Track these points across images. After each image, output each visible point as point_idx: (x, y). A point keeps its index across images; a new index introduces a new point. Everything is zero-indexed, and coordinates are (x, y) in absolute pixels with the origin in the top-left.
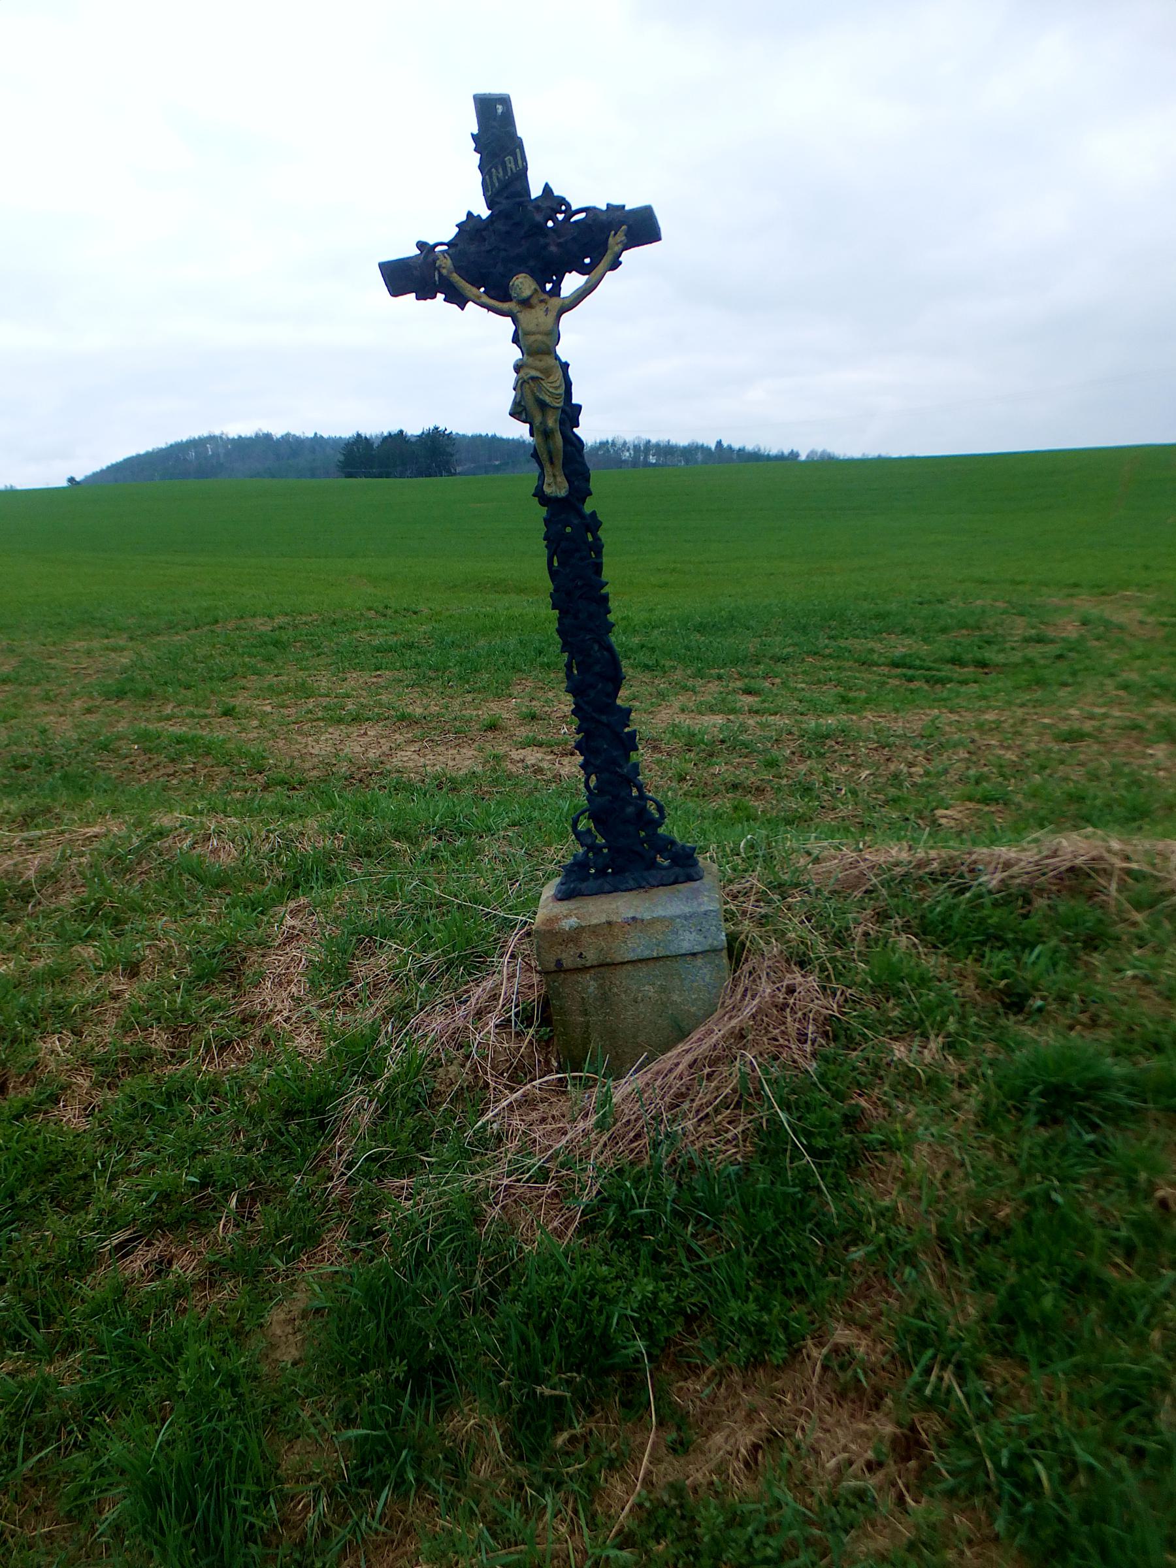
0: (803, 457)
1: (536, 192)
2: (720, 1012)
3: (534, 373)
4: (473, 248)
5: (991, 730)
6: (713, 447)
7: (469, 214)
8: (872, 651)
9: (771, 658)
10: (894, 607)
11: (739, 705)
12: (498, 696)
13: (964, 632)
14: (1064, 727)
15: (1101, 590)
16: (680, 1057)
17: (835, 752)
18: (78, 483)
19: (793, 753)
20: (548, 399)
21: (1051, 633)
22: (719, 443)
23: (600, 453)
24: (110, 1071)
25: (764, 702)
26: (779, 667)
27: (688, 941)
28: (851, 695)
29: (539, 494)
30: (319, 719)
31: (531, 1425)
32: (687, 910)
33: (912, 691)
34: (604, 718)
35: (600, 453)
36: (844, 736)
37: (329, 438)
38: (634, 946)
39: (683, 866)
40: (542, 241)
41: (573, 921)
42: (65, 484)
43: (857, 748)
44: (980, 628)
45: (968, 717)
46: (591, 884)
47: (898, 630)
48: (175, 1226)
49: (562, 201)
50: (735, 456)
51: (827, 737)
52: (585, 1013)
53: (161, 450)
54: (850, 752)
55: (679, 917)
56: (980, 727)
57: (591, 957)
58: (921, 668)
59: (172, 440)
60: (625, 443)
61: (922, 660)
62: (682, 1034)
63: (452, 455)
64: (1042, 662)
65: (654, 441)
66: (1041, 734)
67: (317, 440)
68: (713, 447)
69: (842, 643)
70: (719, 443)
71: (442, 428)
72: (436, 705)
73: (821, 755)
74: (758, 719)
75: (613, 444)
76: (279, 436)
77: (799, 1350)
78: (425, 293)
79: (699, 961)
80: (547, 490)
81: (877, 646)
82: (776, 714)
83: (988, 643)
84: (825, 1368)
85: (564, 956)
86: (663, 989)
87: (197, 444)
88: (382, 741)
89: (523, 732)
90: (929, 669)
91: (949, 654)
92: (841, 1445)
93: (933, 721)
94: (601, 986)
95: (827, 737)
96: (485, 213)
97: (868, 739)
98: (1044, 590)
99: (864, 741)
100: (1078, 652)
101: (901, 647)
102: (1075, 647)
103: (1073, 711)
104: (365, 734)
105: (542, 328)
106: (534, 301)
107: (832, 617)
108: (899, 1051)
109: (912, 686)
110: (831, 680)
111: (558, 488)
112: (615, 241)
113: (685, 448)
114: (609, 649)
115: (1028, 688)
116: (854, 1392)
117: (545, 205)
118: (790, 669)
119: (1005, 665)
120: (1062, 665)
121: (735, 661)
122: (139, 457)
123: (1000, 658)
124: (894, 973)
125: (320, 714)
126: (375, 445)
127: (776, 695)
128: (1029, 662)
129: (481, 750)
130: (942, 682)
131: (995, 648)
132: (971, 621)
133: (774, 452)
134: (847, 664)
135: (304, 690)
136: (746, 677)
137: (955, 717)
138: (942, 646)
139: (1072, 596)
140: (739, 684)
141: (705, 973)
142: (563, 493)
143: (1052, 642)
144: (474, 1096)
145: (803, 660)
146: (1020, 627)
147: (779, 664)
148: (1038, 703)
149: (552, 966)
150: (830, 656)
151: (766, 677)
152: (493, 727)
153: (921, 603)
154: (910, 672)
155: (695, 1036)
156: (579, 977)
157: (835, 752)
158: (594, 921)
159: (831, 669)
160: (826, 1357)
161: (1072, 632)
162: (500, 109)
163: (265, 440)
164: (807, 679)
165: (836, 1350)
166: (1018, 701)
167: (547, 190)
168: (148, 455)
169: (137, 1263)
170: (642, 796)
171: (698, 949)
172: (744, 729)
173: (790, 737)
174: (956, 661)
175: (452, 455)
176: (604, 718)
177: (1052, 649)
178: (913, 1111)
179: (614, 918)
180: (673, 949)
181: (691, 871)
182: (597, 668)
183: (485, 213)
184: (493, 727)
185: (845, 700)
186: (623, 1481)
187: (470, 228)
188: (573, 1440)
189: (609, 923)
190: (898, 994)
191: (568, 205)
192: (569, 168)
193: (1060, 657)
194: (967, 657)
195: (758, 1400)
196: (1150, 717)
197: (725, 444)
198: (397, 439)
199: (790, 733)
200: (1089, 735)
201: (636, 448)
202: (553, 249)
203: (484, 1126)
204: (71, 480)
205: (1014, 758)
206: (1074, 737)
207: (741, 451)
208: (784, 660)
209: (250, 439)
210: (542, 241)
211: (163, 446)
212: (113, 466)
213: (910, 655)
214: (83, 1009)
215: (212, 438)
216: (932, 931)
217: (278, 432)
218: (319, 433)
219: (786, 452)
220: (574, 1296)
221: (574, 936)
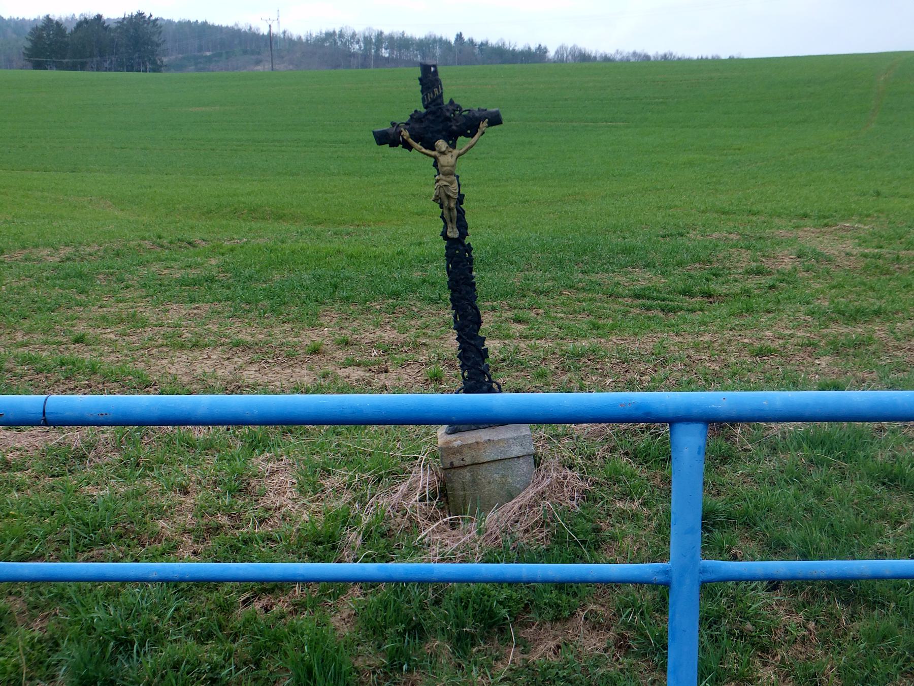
0: (551, 54)
1: (446, 101)
2: (532, 485)
3: (445, 183)
5: (704, 348)
6: (453, 40)
8: (618, 284)
9: (534, 292)
10: (638, 242)
11: (511, 332)
12: (312, 326)
13: (697, 265)
14: (757, 345)
15: (825, 220)
16: (514, 505)
17: (587, 366)
19: (557, 368)
21: (768, 265)
22: (459, 37)
23: (327, 44)
25: (531, 329)
26: (543, 299)
27: (516, 451)
28: (601, 322)
29: (444, 235)
30: (162, 346)
33: (650, 319)
34: (472, 342)
35: (327, 44)
36: (594, 354)
37: (10, 20)
38: (490, 454)
40: (449, 124)
41: (459, 442)
43: (603, 363)
44: (710, 262)
45: (690, 339)
47: (641, 264)
49: (458, 106)
50: (477, 51)
51: (582, 355)
54: (599, 366)
56: (696, 347)
57: (468, 460)
58: (657, 299)
60: (354, 35)
61: (658, 291)
62: (511, 497)
63: (158, 45)
64: (757, 292)
65: (386, 32)
66: (740, 351)
68: (453, 40)
69: (594, 277)
70: (459, 37)
72: (260, 333)
73: (578, 369)
74: (528, 342)
75: (341, 35)
77: (574, 614)
78: (394, 144)
79: (521, 461)
80: (449, 234)
81: (623, 279)
82: (541, 339)
83: (715, 275)
84: (586, 619)
85: (454, 460)
86: (503, 476)
88: (226, 363)
89: (342, 355)
90: (664, 300)
91: (681, 286)
92: (592, 644)
93: (661, 343)
95: (582, 355)
97: (613, 357)
98: (776, 220)
99: (609, 358)
100: (788, 283)
101: (644, 279)
102: (787, 278)
103: (768, 333)
104: (209, 357)
105: (451, 164)
107: (584, 253)
108: (619, 505)
109: (650, 314)
110: (584, 310)
111: (454, 233)
112: (483, 125)
113: (421, 41)
114: (476, 308)
115: (741, 315)
116: (596, 627)
117: (451, 108)
118: (551, 301)
119: (726, 295)
120: (772, 294)
121: (504, 295)
123: (723, 289)
124: (617, 471)
125: (160, 341)
127: (541, 323)
128: (747, 292)
129: (311, 369)
130: (674, 310)
131: (721, 279)
132: (703, 256)
133: (520, 46)
134: (597, 296)
136: (515, 308)
137: (677, 339)
138: (677, 279)
139: (797, 227)
140: (509, 314)
141: (525, 466)
142: (456, 236)
143: (770, 273)
144: (413, 527)
145: (561, 293)
146: (745, 260)
147: (541, 297)
148: (743, 327)
149: (448, 466)
150: (584, 289)
151: (531, 308)
153: (663, 237)
154: (649, 302)
155: (521, 495)
157: (587, 366)
159: (584, 301)
161: (787, 265)
162: (432, 69)
164: (565, 310)
166: (729, 326)
167: (452, 102)
169: (257, 606)
170: (490, 381)
171: (521, 454)
172: (518, 351)
173: (554, 356)
174: (688, 293)
175: (158, 45)
176: (472, 342)
177: (766, 280)
178: (627, 527)
179: (479, 440)
180: (509, 455)
182: (470, 318)
183: (423, 110)
184: (316, 351)
185: (596, 327)
186: (502, 664)
187: (416, 118)
188: (479, 651)
189: (477, 443)
190: (619, 481)
191: (461, 109)
193: (772, 287)
194: (696, 289)
196: (823, 337)
197: (466, 37)
198: (93, 26)
199: (554, 353)
200: (776, 351)
201: (367, 40)
202: (454, 127)
203: (421, 539)
205: (717, 368)
206: (763, 353)
207: (484, 45)
208: (546, 293)
210: (449, 124)
213: (649, 288)
219: (533, 47)
220: (477, 594)
221: (459, 450)
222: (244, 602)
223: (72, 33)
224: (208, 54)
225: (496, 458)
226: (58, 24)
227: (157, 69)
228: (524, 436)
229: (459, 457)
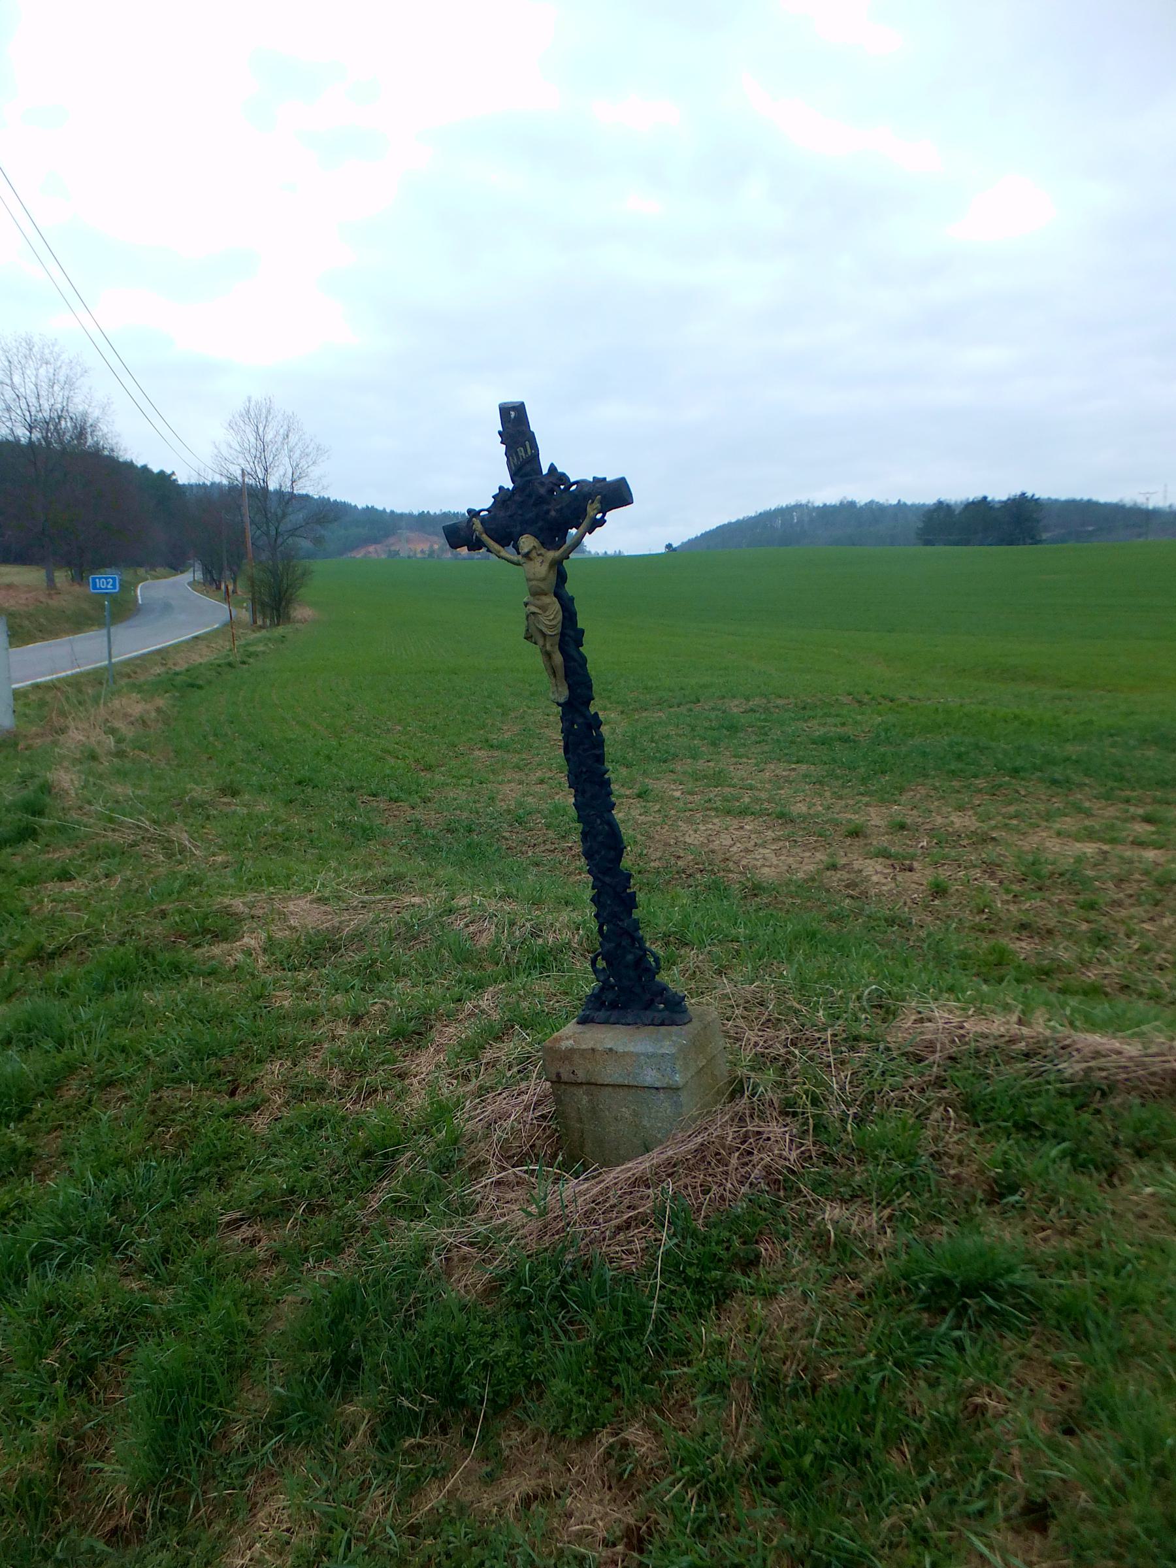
4: (502, 514)
7: (501, 488)
18: (675, 550)
20: (545, 630)
24: (300, 1093)
31: (392, 1425)
32: (651, 1050)
37: (913, 505)
38: (611, 1073)
39: (666, 1009)
42: (662, 550)
46: (602, 1014)
48: (266, 1215)
52: (580, 1121)
53: (751, 518)
55: (643, 1054)
57: (581, 1076)
59: (761, 510)
67: (901, 507)
71: (1029, 494)
76: (862, 503)
79: (662, 1095)
85: (561, 1070)
86: (635, 1114)
87: (783, 513)
92: (595, 1514)
94: (590, 1101)
96: (510, 486)
104: (742, 828)
106: (534, 554)
112: (592, 510)
116: (623, 1480)
122: (730, 524)
126: (957, 512)
135: (718, 778)
152: (855, 833)
156: (574, 1089)
158: (584, 1047)
160: (611, 1446)
163: (848, 508)
165: (625, 1444)
167: (552, 468)
168: (739, 523)
171: (658, 1084)
180: (639, 1081)
181: (677, 1017)
182: (600, 838)
183: (510, 486)
184: (855, 833)
187: (502, 498)
189: (593, 1049)
192: (568, 454)
195: (553, 1462)
198: (980, 508)
204: (669, 546)
209: (834, 506)
211: (753, 514)
212: (707, 533)
214: (304, 1046)
215: (798, 507)
216: (973, 1109)
217: (861, 497)
218: (903, 500)
222: (228, 1224)
223: (960, 514)
224: (1090, 528)
225: (620, 1081)
226: (948, 506)
227: (1037, 542)
228: (663, 1055)
229: (568, 1068)
